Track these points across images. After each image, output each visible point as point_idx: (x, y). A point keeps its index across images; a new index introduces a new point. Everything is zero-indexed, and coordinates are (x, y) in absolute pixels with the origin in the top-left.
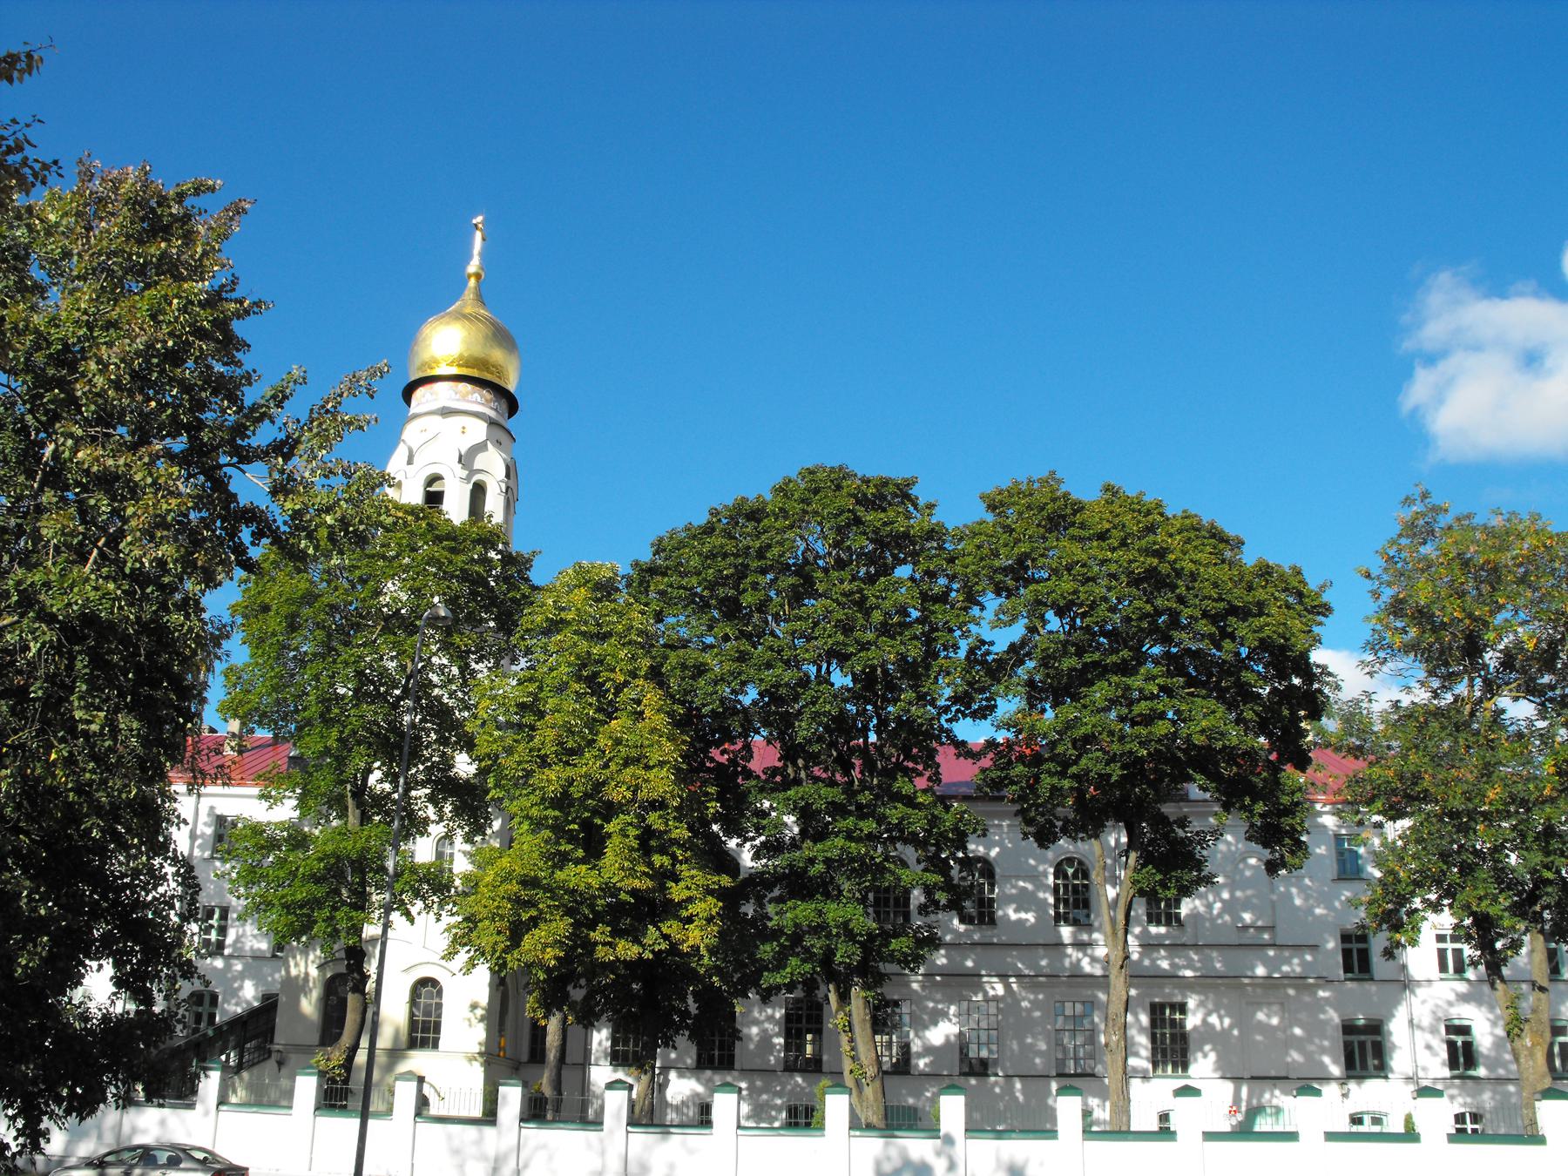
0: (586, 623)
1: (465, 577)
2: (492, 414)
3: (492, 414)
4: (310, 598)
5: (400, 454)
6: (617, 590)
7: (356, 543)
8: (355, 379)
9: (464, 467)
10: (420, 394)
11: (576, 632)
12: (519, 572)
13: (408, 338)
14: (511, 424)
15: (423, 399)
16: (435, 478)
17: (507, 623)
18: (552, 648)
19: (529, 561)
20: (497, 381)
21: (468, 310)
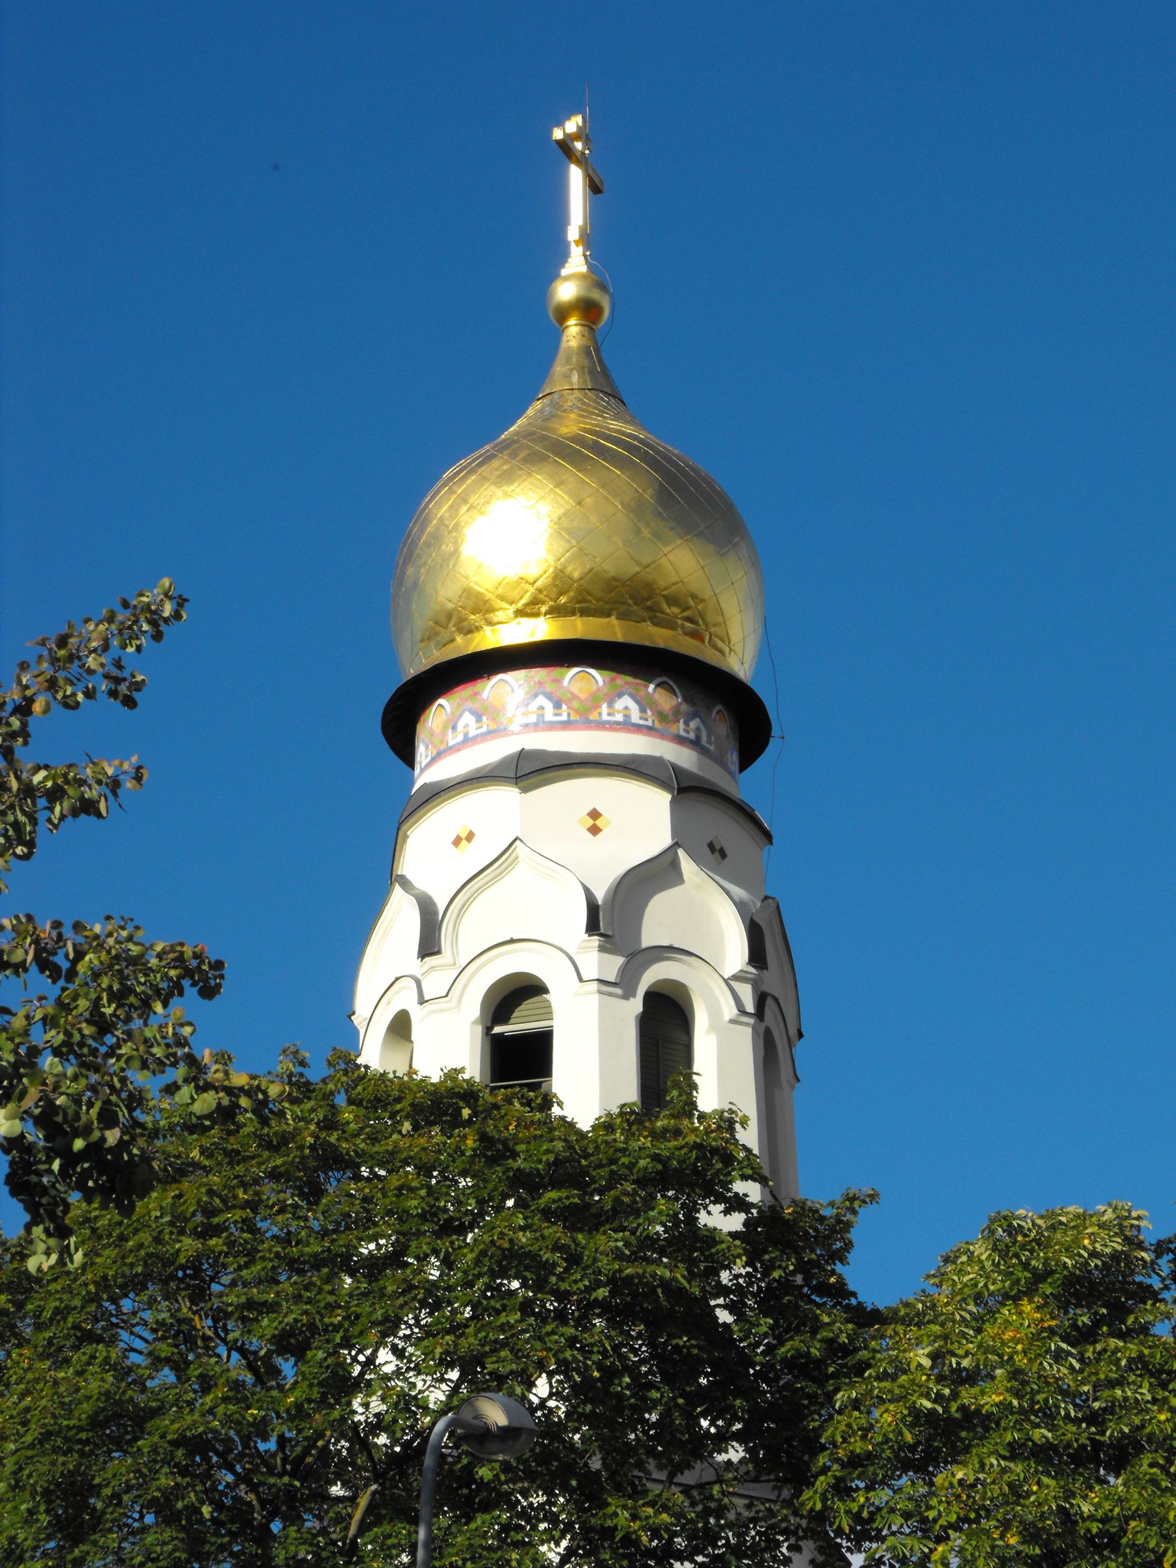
0: (1049, 1416)
1: (629, 1303)
2: (683, 757)
3: (683, 757)
4: (120, 1421)
5: (398, 921)
6: (1147, 1294)
7: (105, 1192)
8: (64, 651)
9: (609, 945)
10: (441, 717)
11: (1014, 1452)
12: (804, 1268)
13: (389, 531)
14: (749, 786)
15: (455, 739)
16: (517, 993)
17: (787, 1451)
18: (942, 1511)
19: (841, 1227)
20: (685, 646)
21: (570, 426)
